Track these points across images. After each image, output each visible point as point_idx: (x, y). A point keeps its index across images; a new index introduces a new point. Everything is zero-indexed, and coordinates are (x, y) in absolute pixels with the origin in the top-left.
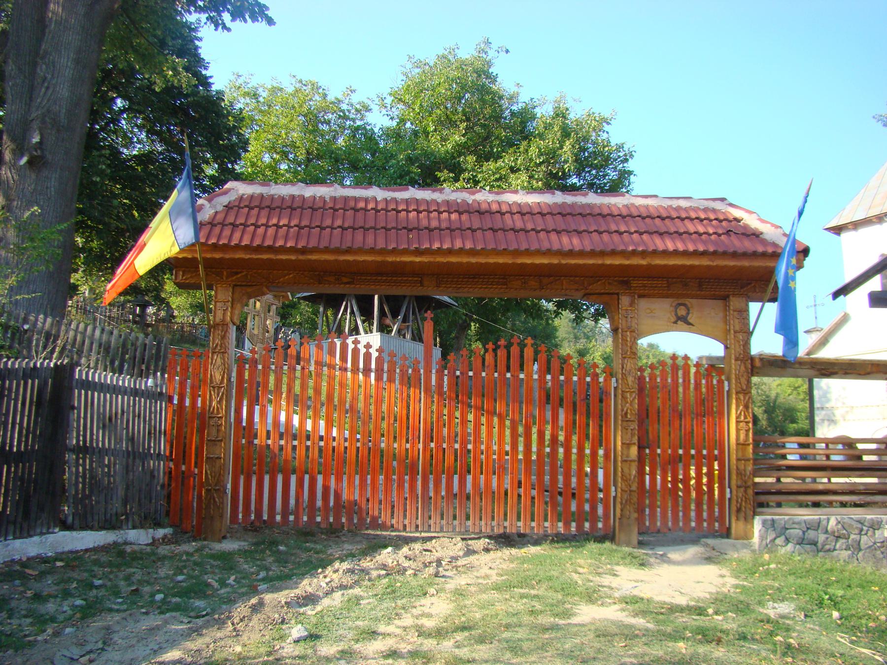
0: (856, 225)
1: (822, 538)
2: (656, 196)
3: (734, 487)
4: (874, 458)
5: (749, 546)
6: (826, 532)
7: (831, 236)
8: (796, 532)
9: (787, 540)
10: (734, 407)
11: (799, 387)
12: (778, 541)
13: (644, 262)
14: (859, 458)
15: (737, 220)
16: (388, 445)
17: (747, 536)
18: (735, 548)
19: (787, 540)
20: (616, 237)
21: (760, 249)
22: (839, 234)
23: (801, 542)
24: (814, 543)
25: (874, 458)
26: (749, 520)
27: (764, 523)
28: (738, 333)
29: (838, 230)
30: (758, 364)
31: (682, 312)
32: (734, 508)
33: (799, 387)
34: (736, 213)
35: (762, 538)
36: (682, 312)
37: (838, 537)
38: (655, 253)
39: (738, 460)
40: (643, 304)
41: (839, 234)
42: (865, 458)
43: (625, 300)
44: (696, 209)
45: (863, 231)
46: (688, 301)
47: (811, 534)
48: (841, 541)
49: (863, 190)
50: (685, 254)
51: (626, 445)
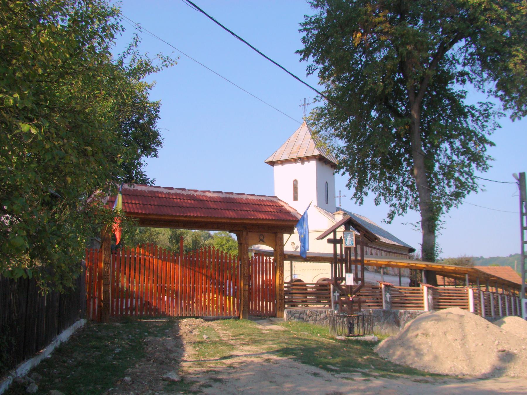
0: (283, 162)
1: (305, 317)
2: (254, 195)
3: (278, 300)
4: (311, 290)
5: (283, 320)
6: (306, 315)
7: (269, 166)
8: (297, 315)
9: (295, 318)
10: (278, 272)
11: (224, 245)
12: (292, 318)
13: (255, 222)
14: (306, 289)
15: (282, 206)
16: (168, 285)
17: (282, 316)
18: (278, 320)
19: (295, 318)
20: (246, 212)
21: (291, 219)
22: (273, 166)
23: (299, 318)
24: (303, 319)
25: (311, 290)
26: (282, 311)
27: (288, 312)
28: (279, 244)
29: (272, 163)
30: (287, 257)
31: (262, 238)
32: (278, 307)
33: (224, 245)
34: (282, 204)
35: (287, 317)
36: (262, 238)
37: (310, 317)
38: (260, 219)
39: (279, 290)
40: (250, 234)
41: (273, 166)
42: (308, 290)
43: (244, 233)
44: (268, 201)
45: (286, 166)
46: (264, 234)
47: (302, 315)
48: (311, 318)
49: (287, 142)
50: (269, 220)
51: (245, 285)
